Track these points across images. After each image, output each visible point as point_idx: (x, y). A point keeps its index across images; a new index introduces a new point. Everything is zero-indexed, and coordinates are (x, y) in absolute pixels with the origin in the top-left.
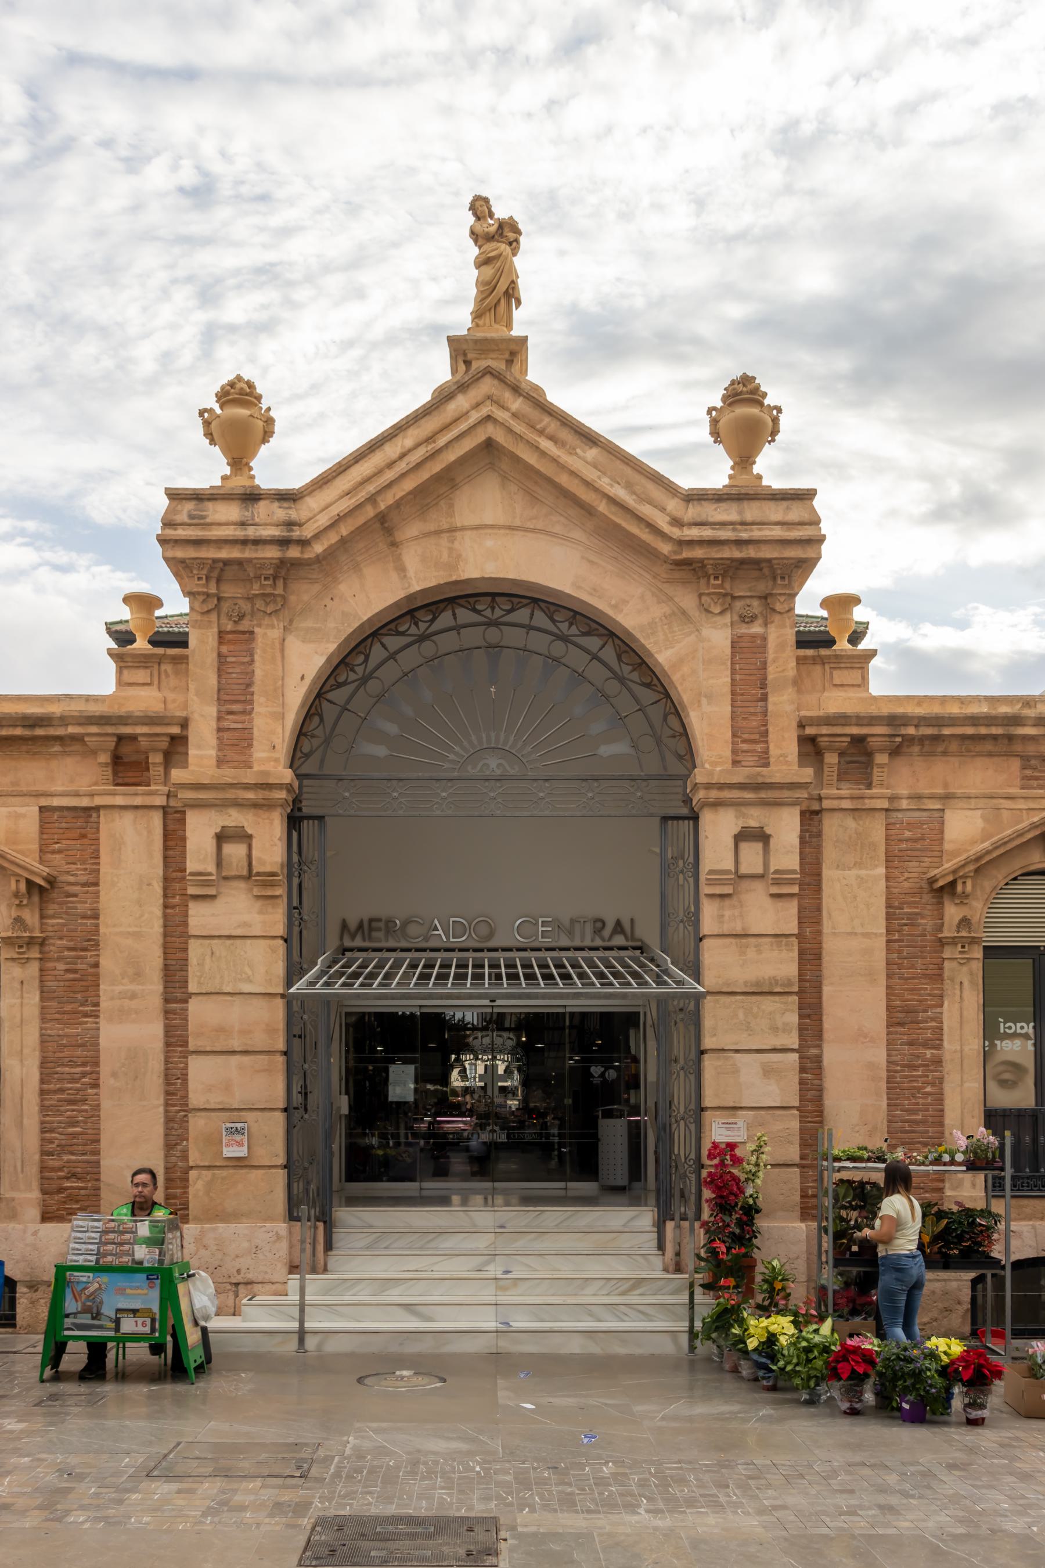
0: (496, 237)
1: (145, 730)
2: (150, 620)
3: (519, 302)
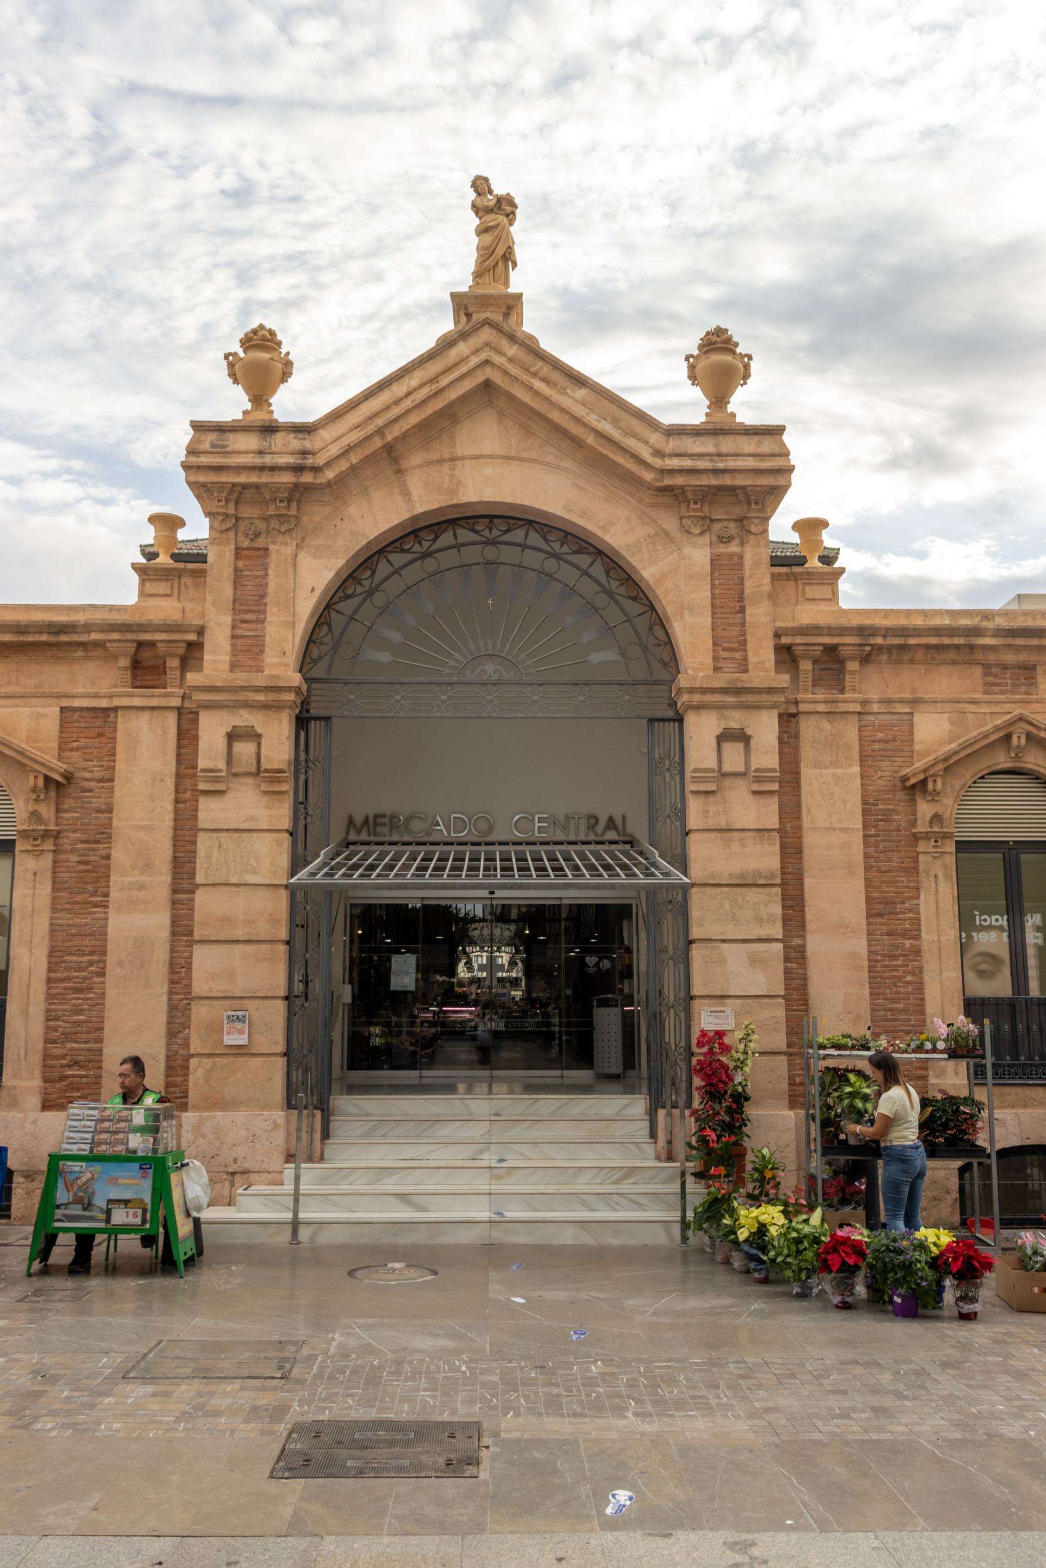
3: (515, 265)
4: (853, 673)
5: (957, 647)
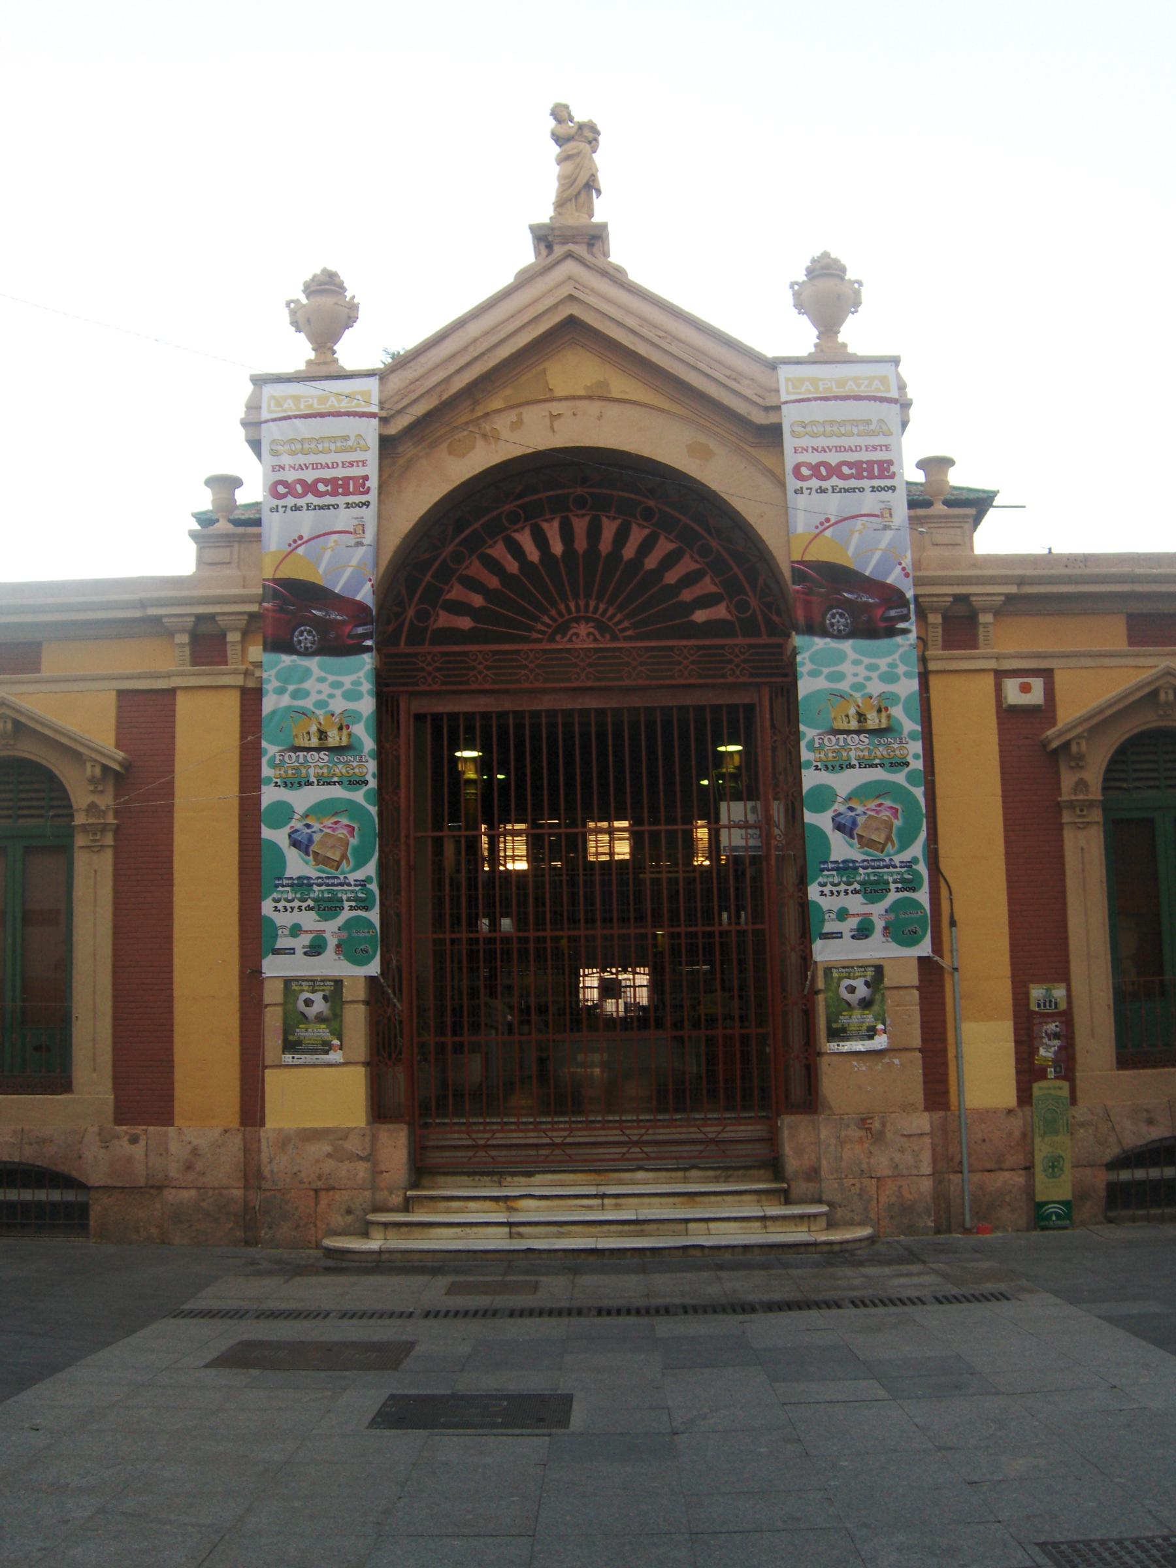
0: (576, 137)
2: (231, 505)
3: (599, 192)
4: (986, 625)
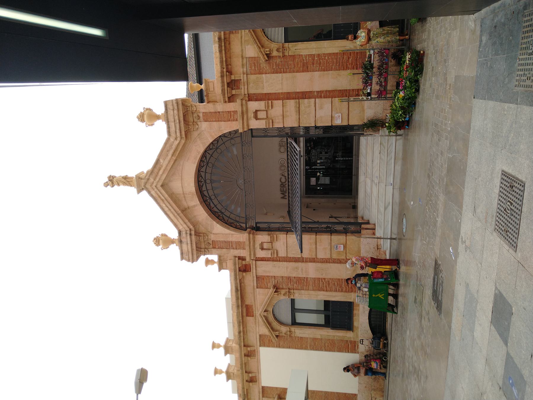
1: (237, 265)
3: (127, 176)
4: (235, 77)
5: (225, 43)
